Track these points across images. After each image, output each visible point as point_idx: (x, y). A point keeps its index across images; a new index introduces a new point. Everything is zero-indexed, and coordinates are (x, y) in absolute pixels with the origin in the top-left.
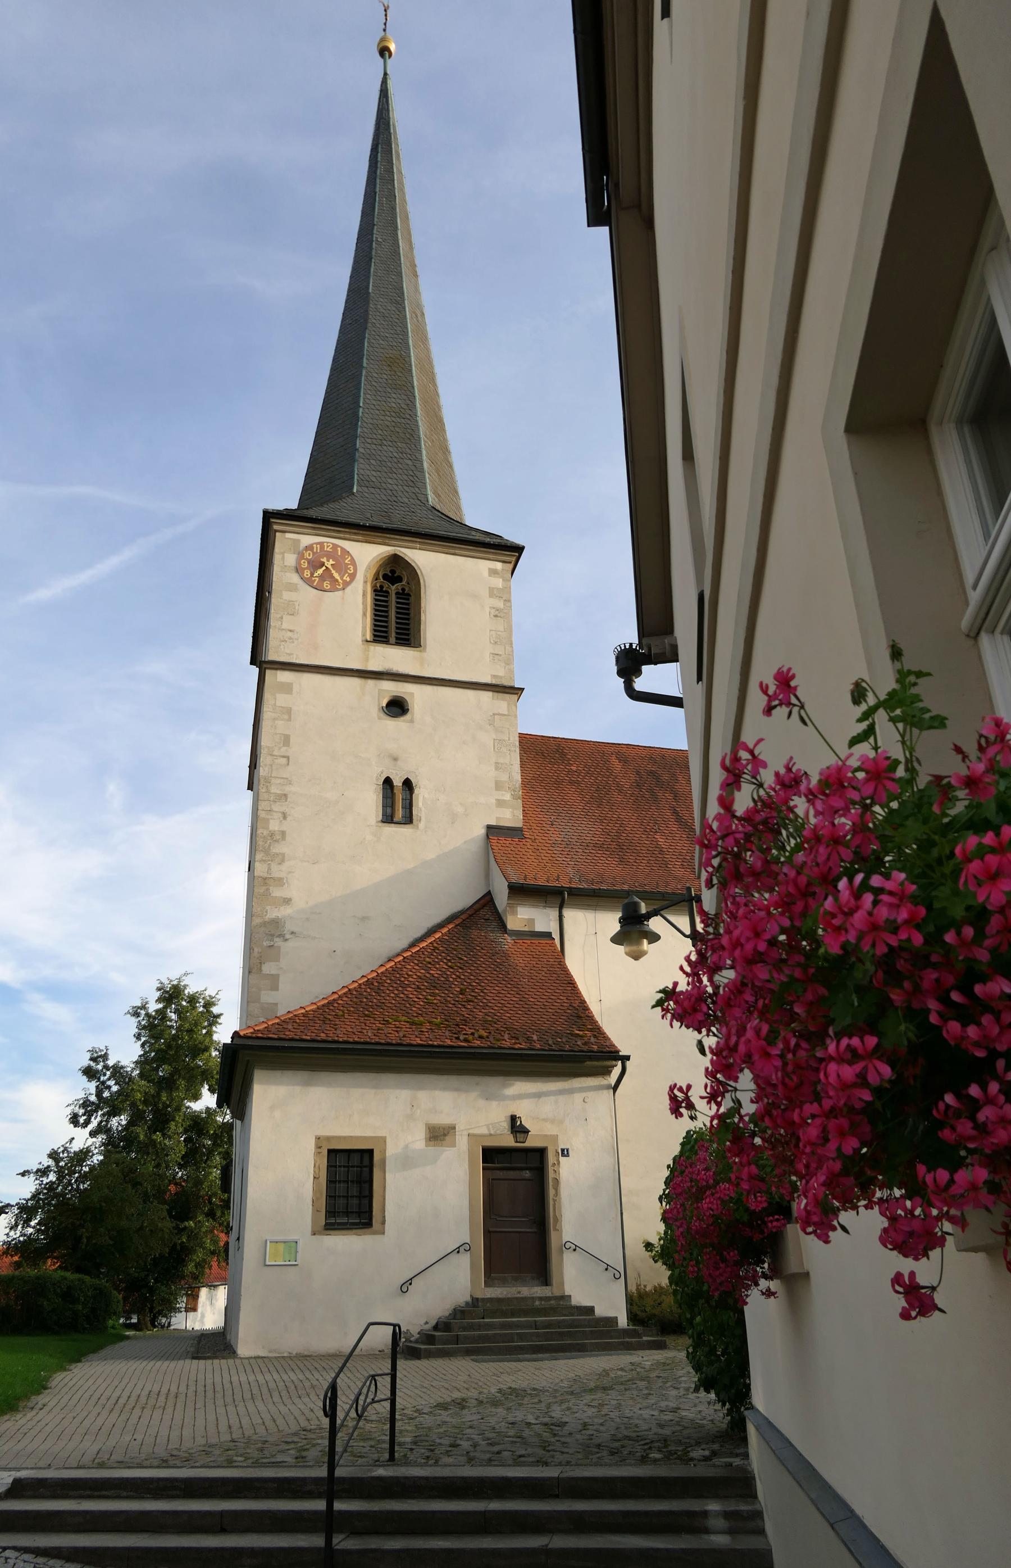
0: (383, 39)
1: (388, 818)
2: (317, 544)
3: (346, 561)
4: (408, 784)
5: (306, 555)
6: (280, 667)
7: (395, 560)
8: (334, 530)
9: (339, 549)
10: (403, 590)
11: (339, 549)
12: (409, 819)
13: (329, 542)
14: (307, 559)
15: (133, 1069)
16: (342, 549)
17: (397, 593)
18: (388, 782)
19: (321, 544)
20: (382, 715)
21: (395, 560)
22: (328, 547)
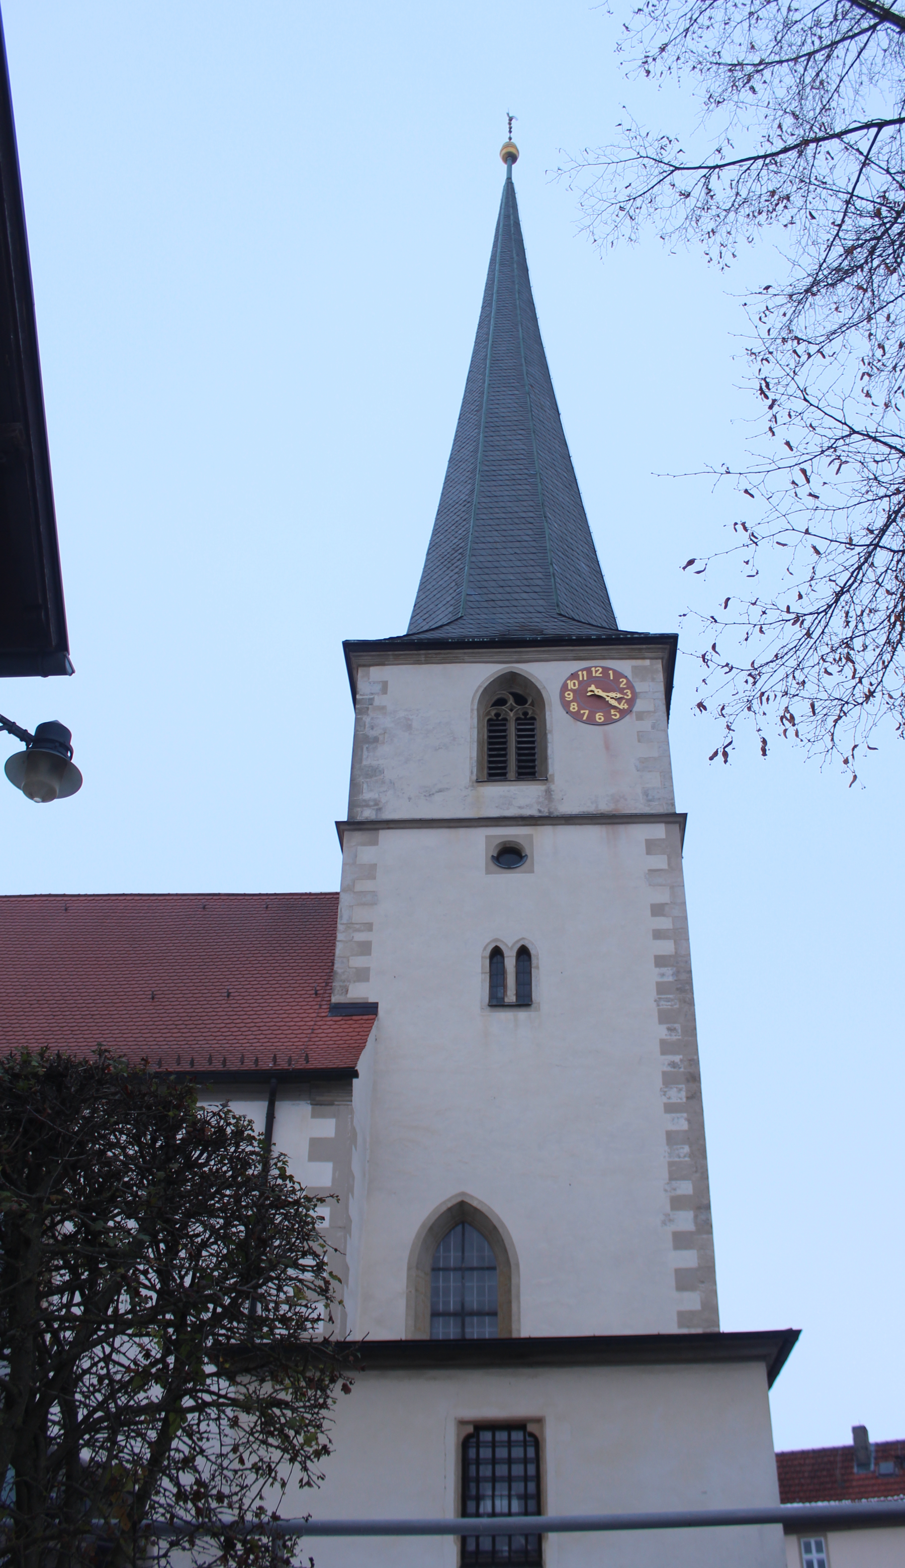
0: (510, 144)
1: (496, 1002)
2: (582, 670)
3: (621, 686)
4: (524, 953)
5: (570, 684)
6: (385, 826)
7: (511, 680)
8: (544, 651)
9: (611, 672)
10: (525, 714)
11: (611, 672)
12: (524, 1001)
13: (597, 667)
14: (572, 690)
15: (268, 1381)
16: (615, 671)
17: (518, 719)
18: (496, 954)
19: (588, 670)
20: (494, 867)
21: (511, 680)
22: (596, 671)
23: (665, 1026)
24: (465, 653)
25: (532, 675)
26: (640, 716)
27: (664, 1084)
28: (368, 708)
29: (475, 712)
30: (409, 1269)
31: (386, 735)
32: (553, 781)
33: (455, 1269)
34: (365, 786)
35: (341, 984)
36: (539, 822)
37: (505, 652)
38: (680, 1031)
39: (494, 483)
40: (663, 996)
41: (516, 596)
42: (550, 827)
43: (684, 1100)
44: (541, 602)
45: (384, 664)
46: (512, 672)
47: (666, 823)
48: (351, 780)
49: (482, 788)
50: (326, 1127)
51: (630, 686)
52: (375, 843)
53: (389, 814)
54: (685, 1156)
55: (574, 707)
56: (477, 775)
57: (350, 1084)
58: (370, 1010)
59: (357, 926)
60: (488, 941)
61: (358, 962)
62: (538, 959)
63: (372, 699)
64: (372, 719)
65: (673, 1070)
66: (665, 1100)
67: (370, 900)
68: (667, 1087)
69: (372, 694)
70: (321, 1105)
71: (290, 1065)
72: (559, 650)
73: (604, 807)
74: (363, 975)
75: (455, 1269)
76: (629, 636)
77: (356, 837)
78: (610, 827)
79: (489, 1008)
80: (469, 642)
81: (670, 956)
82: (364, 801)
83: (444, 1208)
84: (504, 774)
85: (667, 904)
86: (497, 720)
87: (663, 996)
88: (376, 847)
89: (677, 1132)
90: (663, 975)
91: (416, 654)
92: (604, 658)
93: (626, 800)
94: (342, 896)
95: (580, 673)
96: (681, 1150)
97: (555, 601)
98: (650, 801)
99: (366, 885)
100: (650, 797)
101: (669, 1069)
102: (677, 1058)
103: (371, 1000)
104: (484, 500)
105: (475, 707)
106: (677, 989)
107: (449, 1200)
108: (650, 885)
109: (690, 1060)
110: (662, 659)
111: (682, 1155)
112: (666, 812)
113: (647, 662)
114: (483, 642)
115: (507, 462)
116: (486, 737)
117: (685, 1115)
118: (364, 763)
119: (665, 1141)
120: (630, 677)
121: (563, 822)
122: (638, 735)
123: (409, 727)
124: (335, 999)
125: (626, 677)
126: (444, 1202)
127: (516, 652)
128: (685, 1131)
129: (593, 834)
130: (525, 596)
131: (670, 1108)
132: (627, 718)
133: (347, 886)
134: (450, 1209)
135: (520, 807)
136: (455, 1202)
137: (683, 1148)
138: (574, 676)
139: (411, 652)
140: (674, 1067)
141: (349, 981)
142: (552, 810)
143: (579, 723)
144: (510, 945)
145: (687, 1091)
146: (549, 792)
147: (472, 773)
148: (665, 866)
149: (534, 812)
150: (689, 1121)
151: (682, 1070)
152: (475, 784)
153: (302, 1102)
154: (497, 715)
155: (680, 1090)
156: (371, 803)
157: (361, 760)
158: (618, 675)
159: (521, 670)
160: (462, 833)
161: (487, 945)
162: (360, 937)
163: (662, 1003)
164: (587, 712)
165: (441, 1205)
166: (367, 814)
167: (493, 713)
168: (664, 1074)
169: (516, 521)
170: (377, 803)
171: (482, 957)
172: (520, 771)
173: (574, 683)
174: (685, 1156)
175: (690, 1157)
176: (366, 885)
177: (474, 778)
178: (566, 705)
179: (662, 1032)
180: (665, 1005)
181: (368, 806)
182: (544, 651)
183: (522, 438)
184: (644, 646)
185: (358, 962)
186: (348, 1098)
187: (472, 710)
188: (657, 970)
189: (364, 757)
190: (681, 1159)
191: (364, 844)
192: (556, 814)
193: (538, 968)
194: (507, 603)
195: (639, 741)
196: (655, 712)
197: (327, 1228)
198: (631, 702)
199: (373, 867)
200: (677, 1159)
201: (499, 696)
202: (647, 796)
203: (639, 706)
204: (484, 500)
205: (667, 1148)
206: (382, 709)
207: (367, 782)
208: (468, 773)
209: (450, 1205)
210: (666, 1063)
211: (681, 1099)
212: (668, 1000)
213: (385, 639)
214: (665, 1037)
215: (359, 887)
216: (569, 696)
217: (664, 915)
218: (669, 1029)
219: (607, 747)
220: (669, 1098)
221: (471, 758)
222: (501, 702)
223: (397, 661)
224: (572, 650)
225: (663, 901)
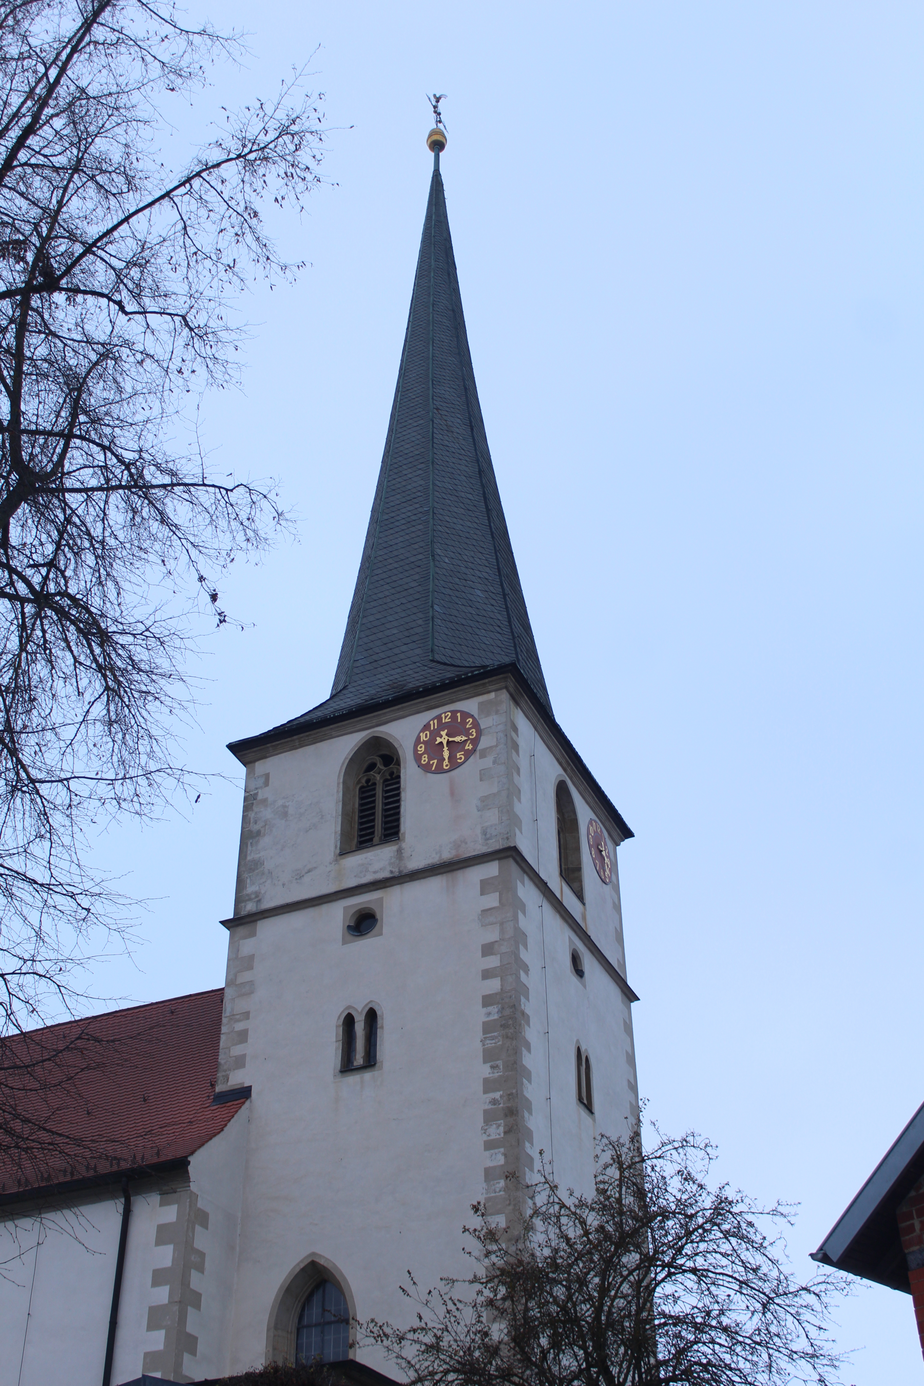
1: (347, 1067)
2: (433, 719)
3: (468, 726)
5: (423, 737)
8: (398, 709)
9: (459, 714)
11: (459, 714)
12: (371, 1062)
13: (445, 713)
16: (462, 713)
18: (349, 1021)
19: (439, 718)
22: (446, 717)
23: (489, 1065)
24: (331, 729)
25: (390, 735)
26: (483, 755)
27: (484, 1123)
28: (253, 804)
29: (341, 786)
30: (268, 1330)
31: (267, 827)
32: (404, 840)
33: (316, 1325)
34: (248, 881)
35: (224, 1074)
36: (388, 884)
37: (365, 719)
38: (501, 1067)
39: (392, 531)
40: (488, 1035)
41: (396, 651)
42: (398, 886)
43: (502, 1135)
44: (418, 651)
45: (265, 757)
46: (374, 737)
47: (499, 859)
48: (237, 878)
49: (344, 860)
50: (170, 1214)
51: (476, 725)
52: (253, 934)
53: (267, 904)
54: (500, 1191)
55: (425, 760)
56: (340, 849)
57: (187, 1172)
58: (244, 1093)
59: (238, 1017)
60: (342, 1009)
61: (237, 1051)
62: (383, 1019)
63: (256, 794)
64: (256, 813)
65: (493, 1107)
66: (485, 1138)
67: (247, 989)
68: (487, 1125)
69: (257, 789)
70: (167, 1193)
71: (143, 1162)
72: (411, 705)
73: (447, 855)
74: (240, 1062)
75: (316, 1325)
76: (470, 674)
77: (241, 931)
78: (450, 875)
79: (340, 1074)
80: (331, 718)
81: (496, 994)
82: (248, 895)
83: (298, 1270)
84: (371, 840)
85: (496, 941)
86: (368, 786)
87: (488, 1035)
88: (255, 938)
89: (494, 1168)
90: (489, 1014)
91: (291, 741)
92: (453, 702)
93: (466, 843)
94: (226, 991)
95: (432, 722)
96: (498, 1185)
97: (430, 646)
98: (488, 839)
99: (245, 977)
100: (488, 836)
101: (490, 1106)
102: (497, 1095)
103: (246, 1085)
104: (381, 553)
105: (341, 780)
106: (501, 1026)
107: (302, 1261)
108: (482, 926)
109: (509, 1095)
110: (506, 688)
111: (498, 1190)
112: (501, 847)
113: (492, 695)
114: (343, 715)
115: (404, 505)
116: (357, 806)
117: (502, 1150)
118: (249, 858)
119: (483, 1178)
120: (476, 716)
121: (408, 879)
122: (480, 774)
123: (285, 815)
124: (219, 1088)
125: (472, 716)
126: (298, 1264)
127: (374, 716)
128: (502, 1166)
129: (435, 884)
130: (404, 648)
131: (489, 1145)
132: (471, 759)
133: (229, 982)
134: (303, 1270)
135: (375, 872)
136: (306, 1262)
137: (499, 1183)
138: (426, 727)
139: (286, 740)
140: (495, 1104)
141: (230, 1070)
142: (401, 869)
143: (429, 775)
144: (360, 1010)
145: (505, 1125)
146: (400, 851)
147: (336, 847)
148: (496, 904)
149: (386, 874)
150: (505, 1155)
151: (501, 1105)
152: (338, 858)
153: (153, 1194)
154: (368, 781)
155: (499, 1126)
156: (253, 896)
157: (246, 856)
158: (465, 715)
159: (382, 732)
160: (325, 909)
161: (341, 1014)
162: (239, 1026)
163: (488, 1042)
164: (436, 761)
165: (295, 1267)
166: (250, 907)
167: (363, 781)
168: (485, 1112)
169: (407, 567)
170: (257, 894)
171: (337, 1026)
172: (386, 833)
173: (426, 734)
174: (500, 1191)
175: (504, 1191)
176: (245, 977)
177: (338, 851)
178: (418, 758)
179: (485, 1071)
180: (490, 1044)
181: (250, 899)
182: (398, 709)
183: (422, 472)
184: (487, 681)
185: (237, 1051)
186: (186, 1184)
187: (338, 784)
188: (485, 1010)
189: (249, 852)
190: (497, 1194)
191: (245, 938)
192: (405, 871)
193: (382, 1027)
194: (387, 661)
195: (481, 780)
196: (496, 746)
197: (165, 1305)
198: (475, 742)
199: (252, 957)
200: (493, 1195)
201: (370, 762)
202: (485, 835)
203: (484, 743)
204: (381, 553)
205: (484, 1185)
206: (265, 801)
207: (250, 877)
208: (332, 848)
209: (302, 1265)
210: (488, 1101)
211: (499, 1135)
212: (493, 1038)
213: (269, 731)
214: (488, 1076)
215: (239, 980)
216: (421, 749)
217: (492, 954)
218: (492, 1067)
219: (452, 793)
220: (489, 1136)
221: (336, 833)
222: (372, 767)
223: (277, 751)
224: (423, 702)
225: (493, 940)
